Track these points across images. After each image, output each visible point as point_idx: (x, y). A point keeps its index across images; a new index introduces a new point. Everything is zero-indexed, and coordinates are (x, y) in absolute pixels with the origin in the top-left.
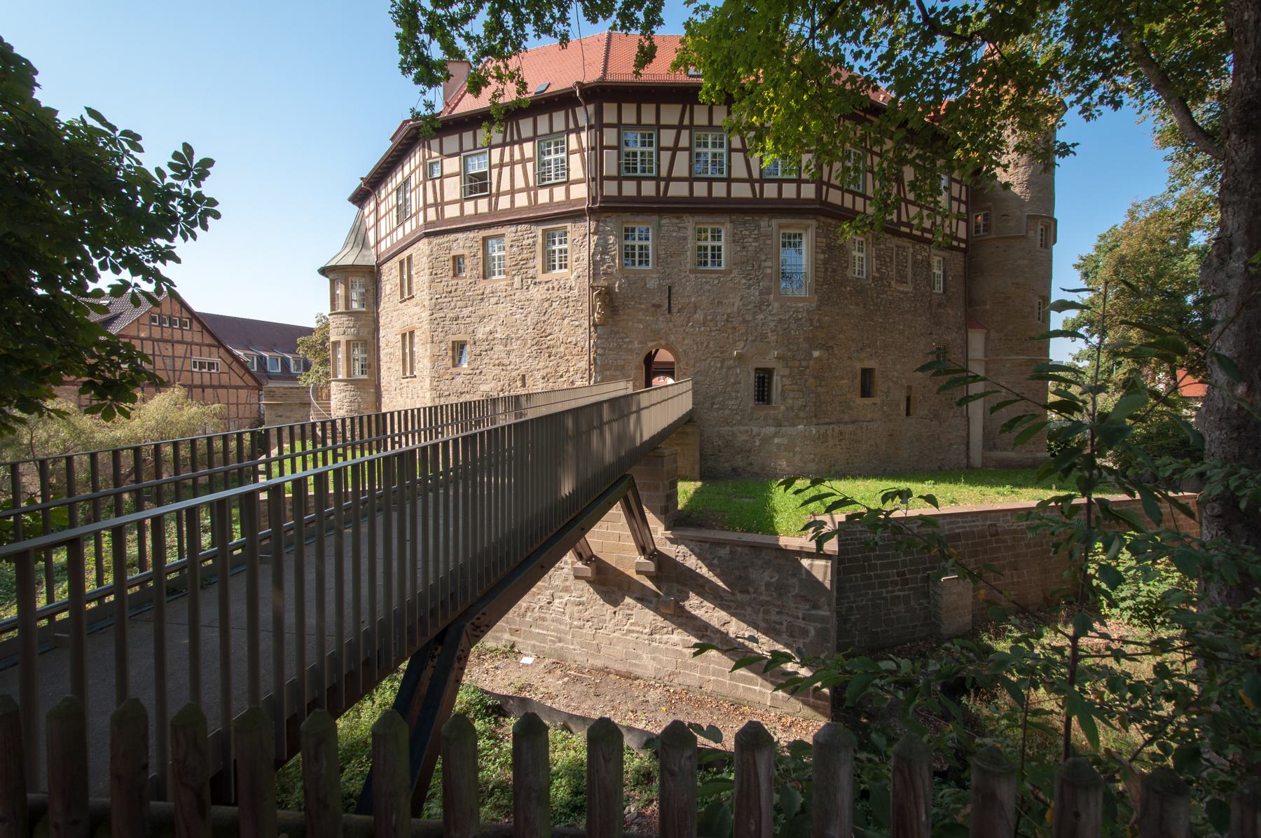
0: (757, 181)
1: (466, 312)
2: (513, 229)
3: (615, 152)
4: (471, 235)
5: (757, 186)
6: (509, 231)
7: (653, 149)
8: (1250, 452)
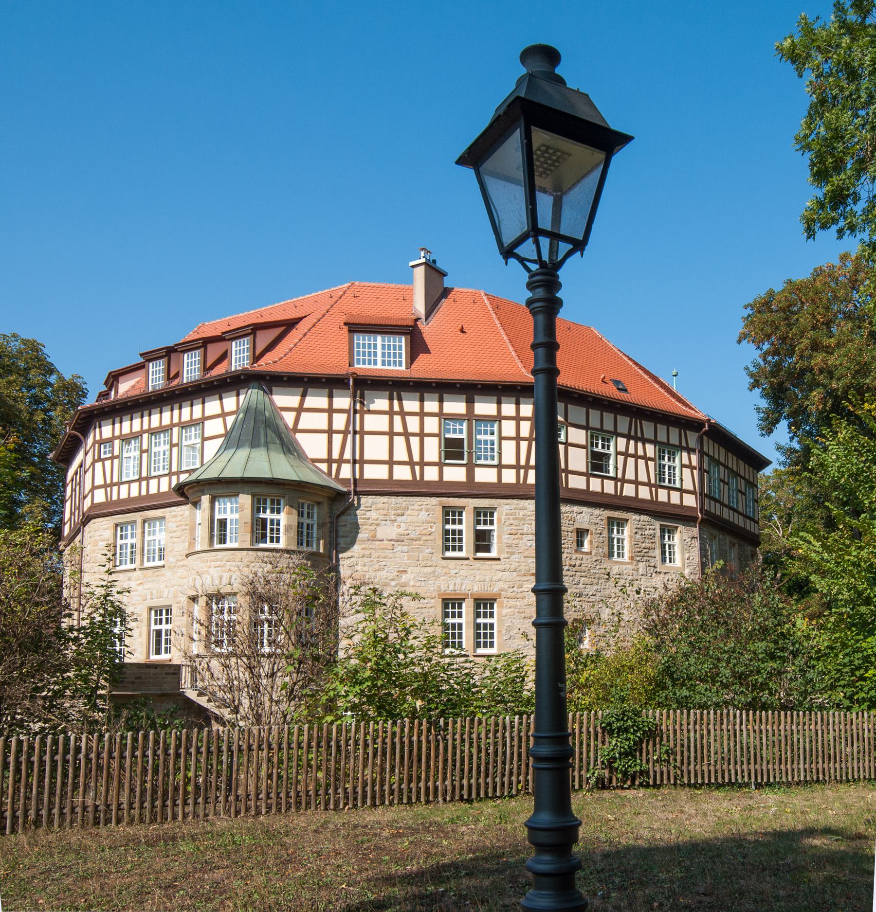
0: (417, 464)
1: (590, 590)
2: (637, 517)
3: (503, 435)
4: (597, 512)
5: (417, 468)
6: (633, 517)
7: (495, 438)
8: (130, 734)
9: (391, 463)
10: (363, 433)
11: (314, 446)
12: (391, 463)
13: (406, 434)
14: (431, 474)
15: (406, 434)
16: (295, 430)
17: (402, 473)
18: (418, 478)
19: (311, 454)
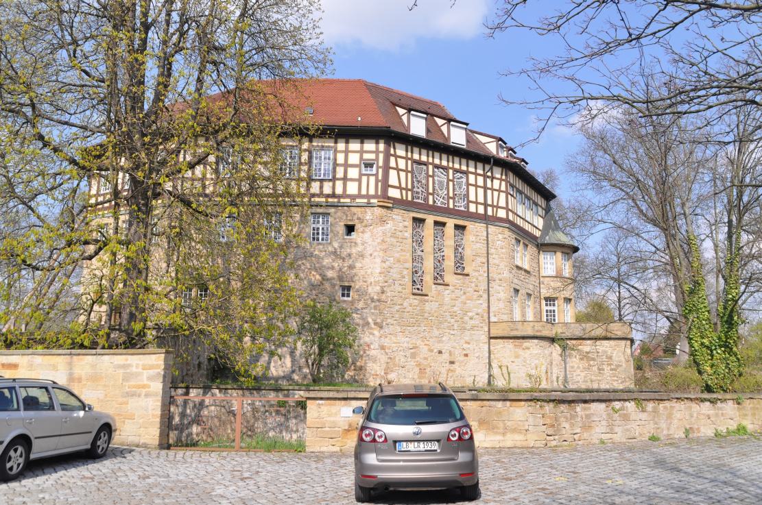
18: (404, 198)
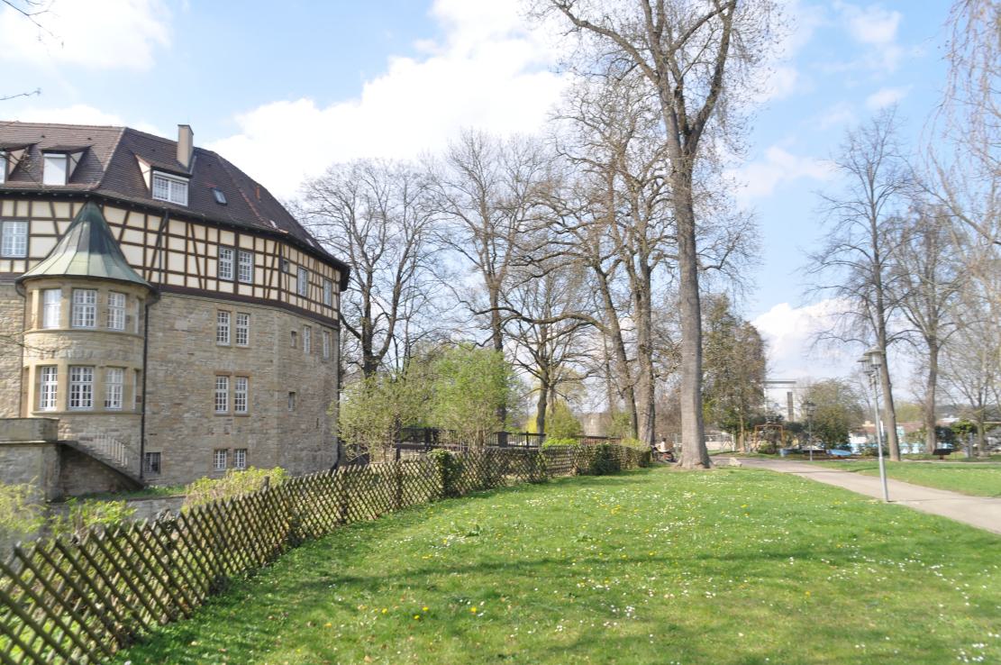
9: (186, 274)
10: (167, 250)
11: (134, 255)
12: (186, 274)
13: (197, 255)
14: (212, 286)
15: (197, 255)
16: (120, 242)
17: (193, 283)
19: (131, 262)
